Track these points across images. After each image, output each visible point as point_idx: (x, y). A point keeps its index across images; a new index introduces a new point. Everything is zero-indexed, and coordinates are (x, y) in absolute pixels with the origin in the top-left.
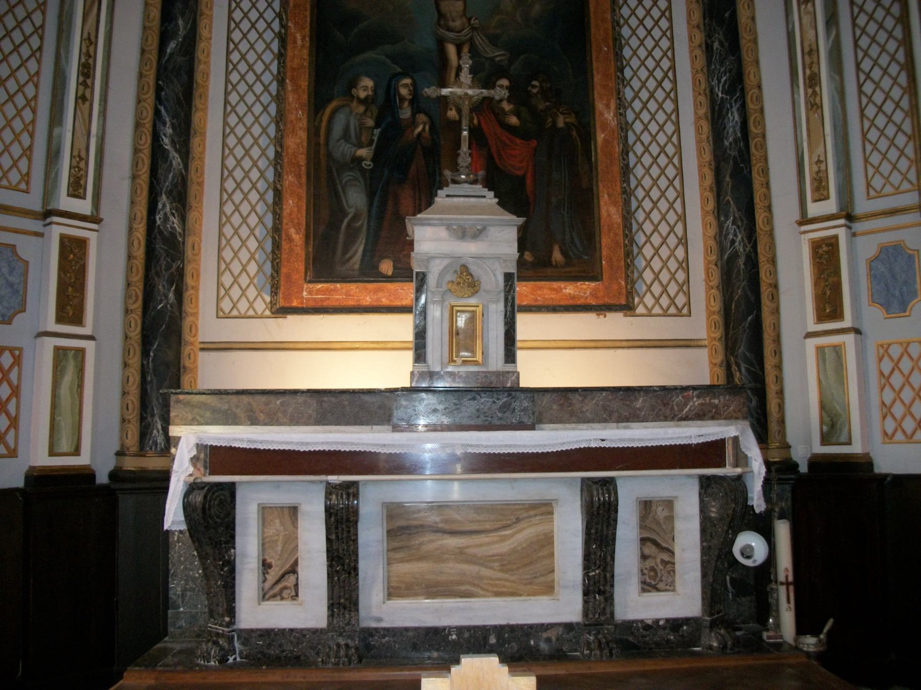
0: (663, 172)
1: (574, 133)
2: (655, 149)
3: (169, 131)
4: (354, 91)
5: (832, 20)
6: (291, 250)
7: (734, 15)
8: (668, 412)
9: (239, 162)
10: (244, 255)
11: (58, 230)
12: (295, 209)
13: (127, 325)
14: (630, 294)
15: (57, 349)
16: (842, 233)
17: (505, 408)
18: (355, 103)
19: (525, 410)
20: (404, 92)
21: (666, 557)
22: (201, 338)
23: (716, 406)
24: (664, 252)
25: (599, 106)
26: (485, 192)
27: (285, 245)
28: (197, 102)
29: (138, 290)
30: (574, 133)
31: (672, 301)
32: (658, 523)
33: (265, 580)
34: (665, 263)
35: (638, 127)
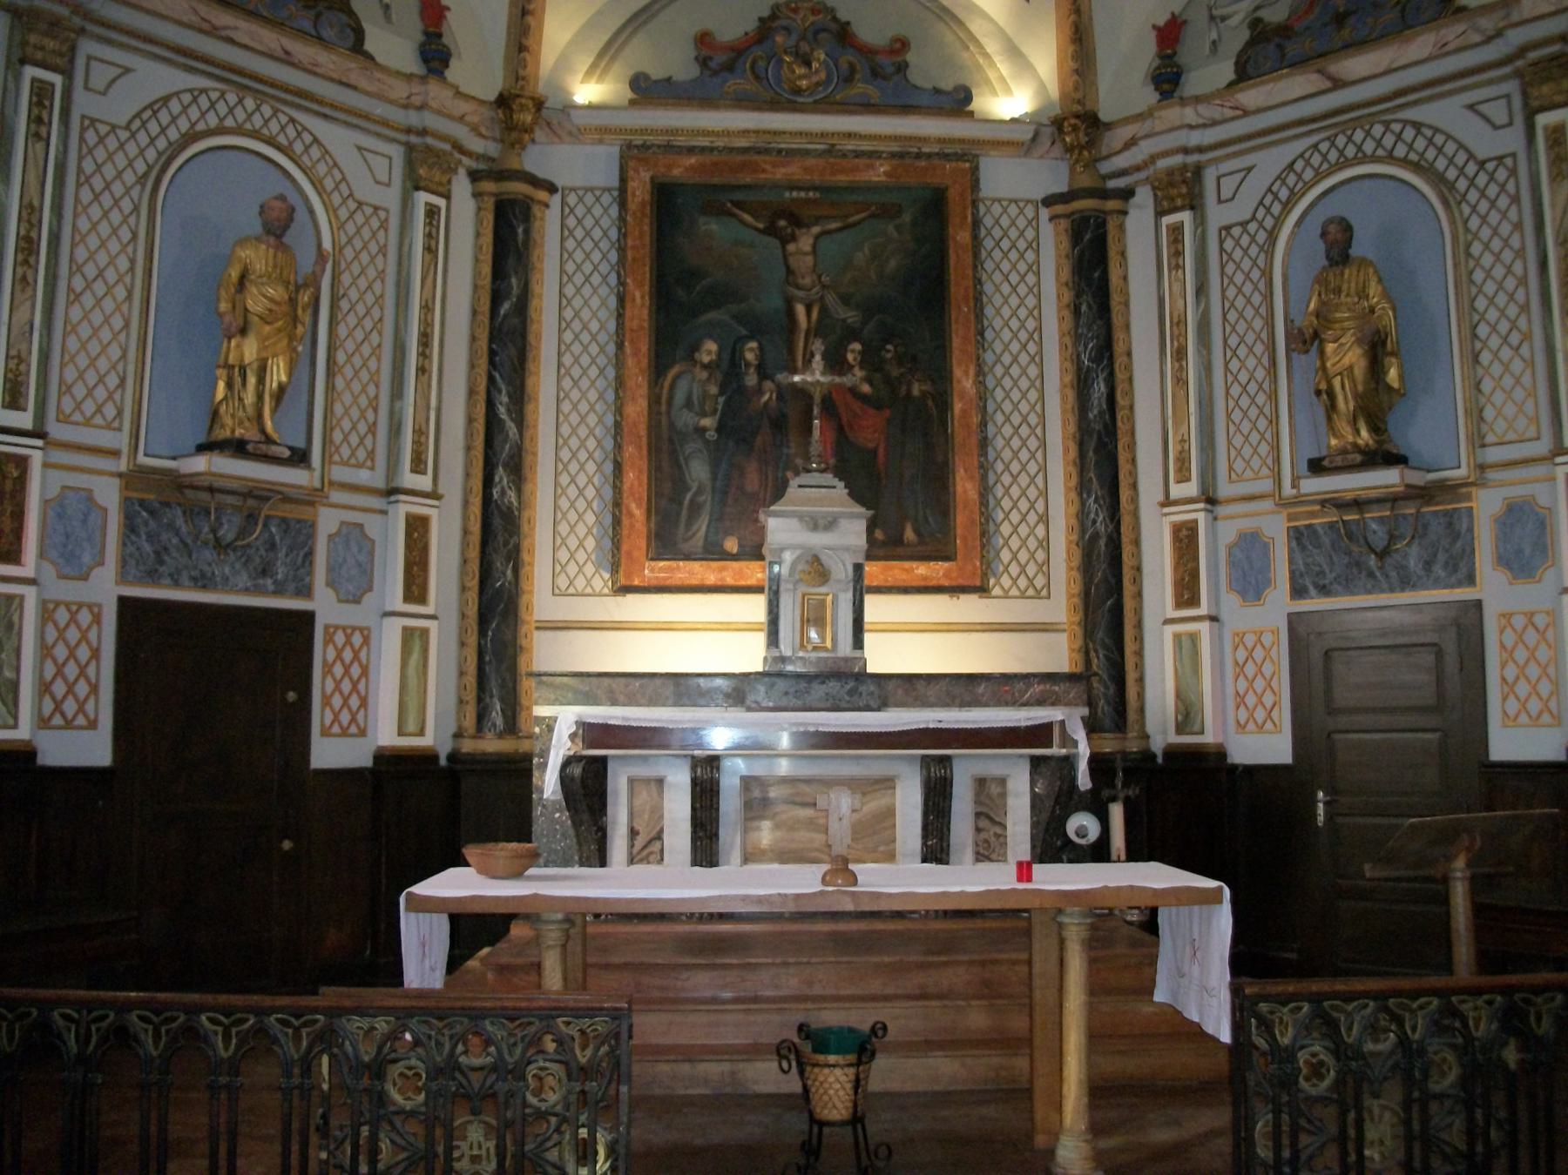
0: (1024, 443)
1: (930, 403)
2: (1016, 419)
3: (505, 399)
4: (697, 355)
5: (1201, 290)
6: (632, 526)
7: (1105, 272)
8: (1009, 698)
9: (574, 431)
10: (581, 530)
11: (405, 507)
12: (636, 483)
13: (463, 603)
14: (985, 576)
15: (405, 629)
16: (1201, 517)
17: (851, 693)
18: (697, 370)
19: (872, 693)
20: (750, 356)
21: (998, 830)
22: (536, 617)
23: (1056, 693)
24: (1023, 530)
25: (958, 372)
26: (836, 482)
27: (625, 521)
28: (530, 365)
29: (475, 566)
30: (930, 403)
31: (1031, 581)
32: (989, 796)
33: (633, 846)
34: (1024, 542)
35: (999, 394)
